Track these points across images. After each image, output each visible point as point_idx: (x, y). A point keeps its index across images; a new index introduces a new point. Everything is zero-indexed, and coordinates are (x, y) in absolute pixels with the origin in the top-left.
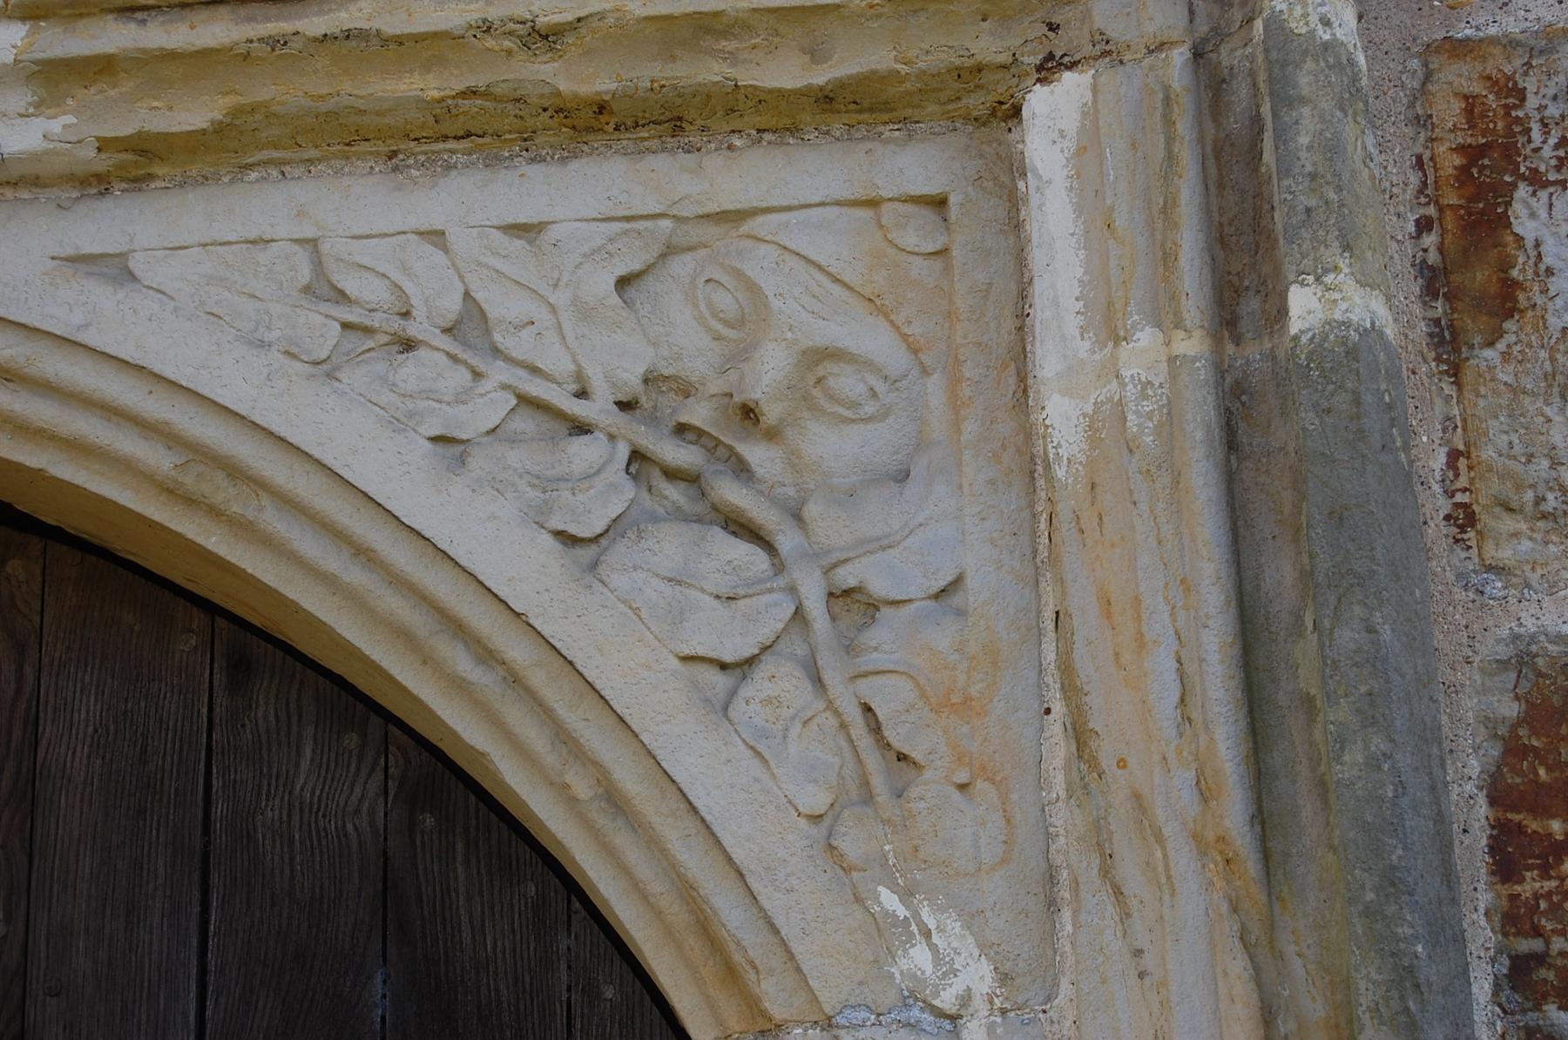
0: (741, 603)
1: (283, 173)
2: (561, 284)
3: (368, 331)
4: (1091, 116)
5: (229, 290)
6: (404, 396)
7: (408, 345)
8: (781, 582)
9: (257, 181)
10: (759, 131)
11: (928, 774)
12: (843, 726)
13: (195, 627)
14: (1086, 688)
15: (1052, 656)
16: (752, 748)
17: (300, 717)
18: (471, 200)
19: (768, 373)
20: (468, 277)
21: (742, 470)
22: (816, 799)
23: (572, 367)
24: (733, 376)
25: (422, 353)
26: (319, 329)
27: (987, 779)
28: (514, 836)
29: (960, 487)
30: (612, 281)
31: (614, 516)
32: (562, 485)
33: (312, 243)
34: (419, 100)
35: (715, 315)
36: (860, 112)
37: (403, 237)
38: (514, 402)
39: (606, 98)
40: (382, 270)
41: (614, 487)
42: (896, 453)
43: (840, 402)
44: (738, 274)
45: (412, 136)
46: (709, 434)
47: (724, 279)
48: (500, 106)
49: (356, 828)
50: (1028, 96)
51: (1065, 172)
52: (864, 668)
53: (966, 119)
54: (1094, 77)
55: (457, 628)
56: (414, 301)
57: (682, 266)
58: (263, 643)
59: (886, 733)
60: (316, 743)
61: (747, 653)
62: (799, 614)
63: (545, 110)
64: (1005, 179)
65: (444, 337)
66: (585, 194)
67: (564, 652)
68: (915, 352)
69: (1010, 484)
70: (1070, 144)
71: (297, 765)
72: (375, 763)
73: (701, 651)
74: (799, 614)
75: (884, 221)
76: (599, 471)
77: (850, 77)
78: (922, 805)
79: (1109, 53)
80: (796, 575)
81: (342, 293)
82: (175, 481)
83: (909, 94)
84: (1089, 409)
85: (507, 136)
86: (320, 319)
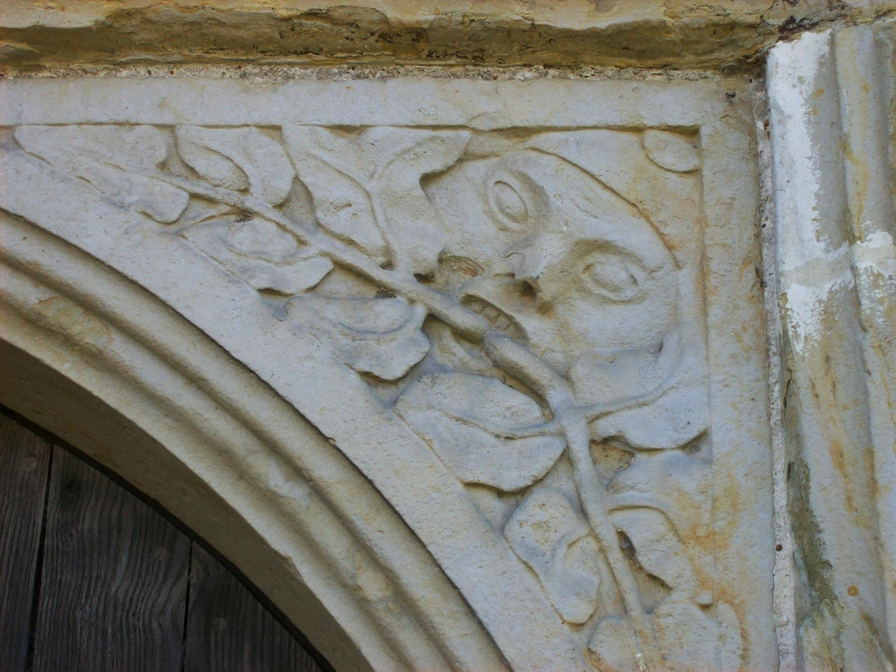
0: (518, 443)
1: (150, 73)
2: (376, 176)
3: (211, 201)
4: (829, 65)
5: (98, 160)
6: (240, 254)
7: (245, 215)
8: (552, 427)
9: (128, 77)
10: (546, 66)
11: (675, 595)
12: (602, 550)
13: (36, 452)
14: (821, 527)
15: (784, 502)
16: (524, 563)
17: (119, 532)
18: (306, 100)
19: (546, 256)
20: (299, 165)
21: (520, 335)
22: (580, 611)
23: (381, 243)
24: (515, 260)
25: (256, 221)
26: (171, 197)
27: (726, 602)
28: (293, 642)
29: (707, 359)
30: (418, 177)
31: (412, 364)
32: (369, 336)
33: (170, 128)
34: (269, 16)
35: (502, 210)
36: (630, 57)
37: (246, 129)
38: (331, 266)
39: (425, 26)
40: (226, 153)
41: (412, 341)
42: (650, 330)
43: (604, 286)
44: (525, 179)
45: (260, 49)
46: (492, 306)
47: (512, 181)
48: (336, 28)
49: (160, 626)
50: (772, 50)
51: (803, 110)
52: (621, 503)
53: (715, 68)
54: (831, 34)
55: (273, 448)
56: (252, 180)
57: (475, 170)
58: (92, 469)
59: (640, 558)
60: (131, 553)
61: (522, 484)
62: (566, 456)
63: (372, 34)
64: (746, 118)
65: (276, 211)
66: (403, 102)
67: (366, 472)
68: (670, 248)
69: (748, 359)
70: (808, 88)
71: (114, 571)
72: (180, 573)
73: (483, 479)
74: (566, 456)
75: (647, 144)
76: (400, 328)
77: (626, 25)
78: (670, 620)
79: (845, 16)
80: (565, 422)
81: (192, 170)
82: (39, 314)
83: (674, 43)
84: (824, 297)
85: (339, 55)
86: (172, 189)
